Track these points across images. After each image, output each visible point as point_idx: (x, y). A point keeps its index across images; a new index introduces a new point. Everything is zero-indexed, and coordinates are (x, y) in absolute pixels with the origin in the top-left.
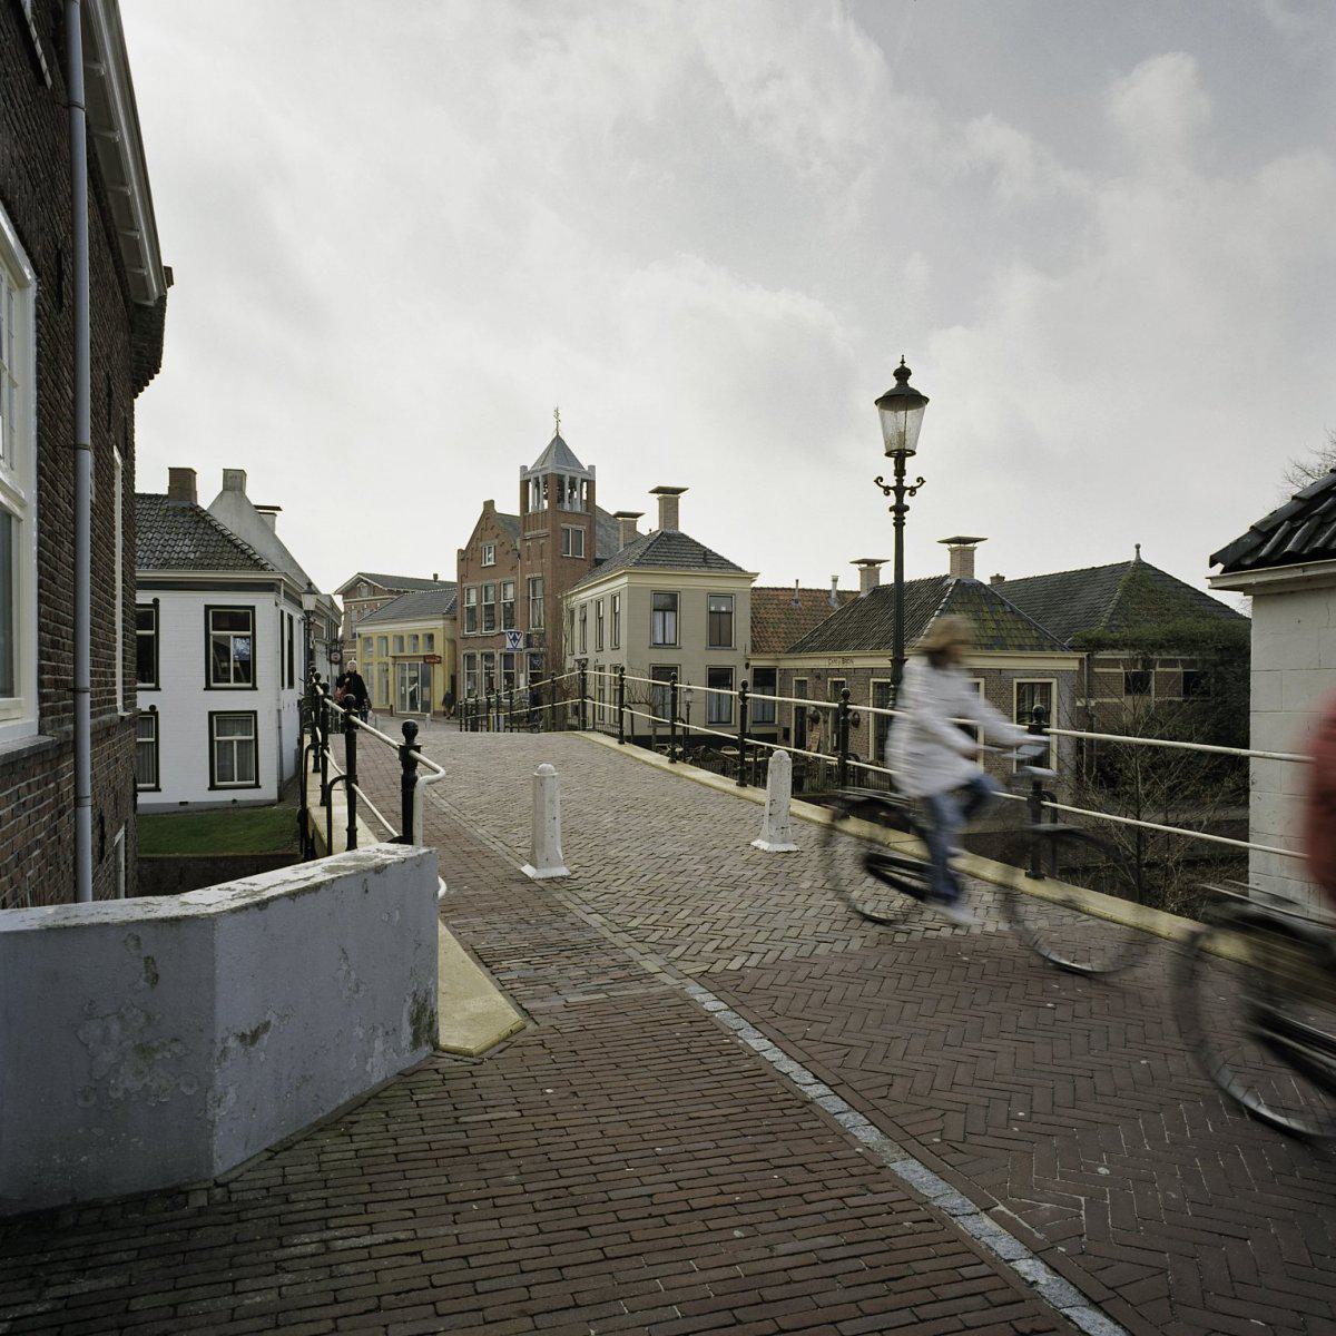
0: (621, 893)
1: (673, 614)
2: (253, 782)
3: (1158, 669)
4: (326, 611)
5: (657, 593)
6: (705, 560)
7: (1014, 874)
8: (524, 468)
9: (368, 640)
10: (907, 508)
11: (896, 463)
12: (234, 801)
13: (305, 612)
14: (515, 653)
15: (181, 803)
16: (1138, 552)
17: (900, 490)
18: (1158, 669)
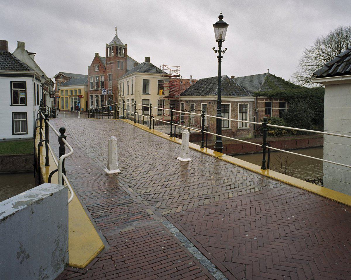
0: (138, 179)
2: (26, 133)
3: (273, 101)
4: (49, 83)
6: (157, 70)
7: (265, 172)
8: (107, 44)
9: (62, 91)
10: (222, 57)
11: (219, 43)
12: (20, 138)
13: (42, 83)
14: (104, 95)
15: (3, 139)
16: (268, 71)
17: (220, 52)
18: (273, 101)
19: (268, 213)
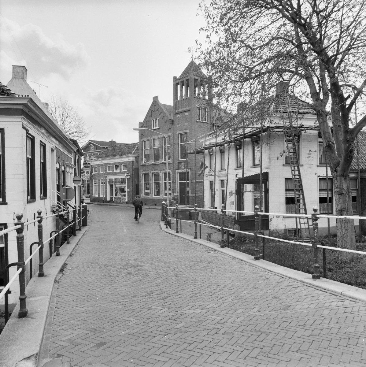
8: (175, 78)
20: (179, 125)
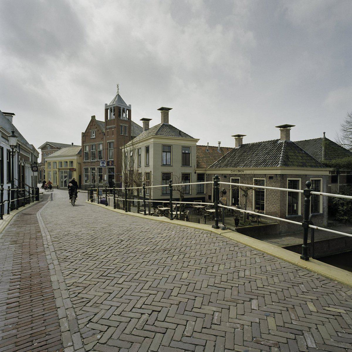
1: (169, 153)
5: (164, 146)
6: (180, 134)
16: (324, 135)
19: (275, 273)
20: (108, 137)
